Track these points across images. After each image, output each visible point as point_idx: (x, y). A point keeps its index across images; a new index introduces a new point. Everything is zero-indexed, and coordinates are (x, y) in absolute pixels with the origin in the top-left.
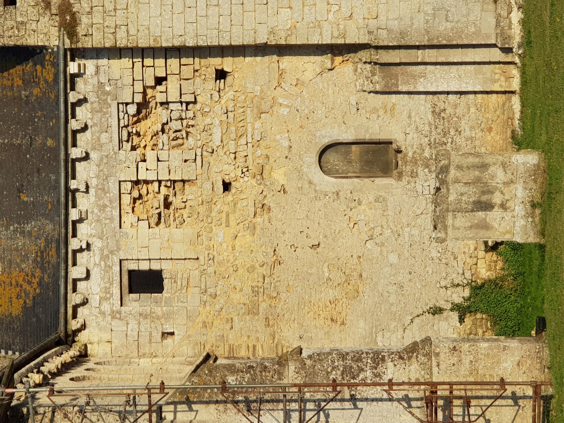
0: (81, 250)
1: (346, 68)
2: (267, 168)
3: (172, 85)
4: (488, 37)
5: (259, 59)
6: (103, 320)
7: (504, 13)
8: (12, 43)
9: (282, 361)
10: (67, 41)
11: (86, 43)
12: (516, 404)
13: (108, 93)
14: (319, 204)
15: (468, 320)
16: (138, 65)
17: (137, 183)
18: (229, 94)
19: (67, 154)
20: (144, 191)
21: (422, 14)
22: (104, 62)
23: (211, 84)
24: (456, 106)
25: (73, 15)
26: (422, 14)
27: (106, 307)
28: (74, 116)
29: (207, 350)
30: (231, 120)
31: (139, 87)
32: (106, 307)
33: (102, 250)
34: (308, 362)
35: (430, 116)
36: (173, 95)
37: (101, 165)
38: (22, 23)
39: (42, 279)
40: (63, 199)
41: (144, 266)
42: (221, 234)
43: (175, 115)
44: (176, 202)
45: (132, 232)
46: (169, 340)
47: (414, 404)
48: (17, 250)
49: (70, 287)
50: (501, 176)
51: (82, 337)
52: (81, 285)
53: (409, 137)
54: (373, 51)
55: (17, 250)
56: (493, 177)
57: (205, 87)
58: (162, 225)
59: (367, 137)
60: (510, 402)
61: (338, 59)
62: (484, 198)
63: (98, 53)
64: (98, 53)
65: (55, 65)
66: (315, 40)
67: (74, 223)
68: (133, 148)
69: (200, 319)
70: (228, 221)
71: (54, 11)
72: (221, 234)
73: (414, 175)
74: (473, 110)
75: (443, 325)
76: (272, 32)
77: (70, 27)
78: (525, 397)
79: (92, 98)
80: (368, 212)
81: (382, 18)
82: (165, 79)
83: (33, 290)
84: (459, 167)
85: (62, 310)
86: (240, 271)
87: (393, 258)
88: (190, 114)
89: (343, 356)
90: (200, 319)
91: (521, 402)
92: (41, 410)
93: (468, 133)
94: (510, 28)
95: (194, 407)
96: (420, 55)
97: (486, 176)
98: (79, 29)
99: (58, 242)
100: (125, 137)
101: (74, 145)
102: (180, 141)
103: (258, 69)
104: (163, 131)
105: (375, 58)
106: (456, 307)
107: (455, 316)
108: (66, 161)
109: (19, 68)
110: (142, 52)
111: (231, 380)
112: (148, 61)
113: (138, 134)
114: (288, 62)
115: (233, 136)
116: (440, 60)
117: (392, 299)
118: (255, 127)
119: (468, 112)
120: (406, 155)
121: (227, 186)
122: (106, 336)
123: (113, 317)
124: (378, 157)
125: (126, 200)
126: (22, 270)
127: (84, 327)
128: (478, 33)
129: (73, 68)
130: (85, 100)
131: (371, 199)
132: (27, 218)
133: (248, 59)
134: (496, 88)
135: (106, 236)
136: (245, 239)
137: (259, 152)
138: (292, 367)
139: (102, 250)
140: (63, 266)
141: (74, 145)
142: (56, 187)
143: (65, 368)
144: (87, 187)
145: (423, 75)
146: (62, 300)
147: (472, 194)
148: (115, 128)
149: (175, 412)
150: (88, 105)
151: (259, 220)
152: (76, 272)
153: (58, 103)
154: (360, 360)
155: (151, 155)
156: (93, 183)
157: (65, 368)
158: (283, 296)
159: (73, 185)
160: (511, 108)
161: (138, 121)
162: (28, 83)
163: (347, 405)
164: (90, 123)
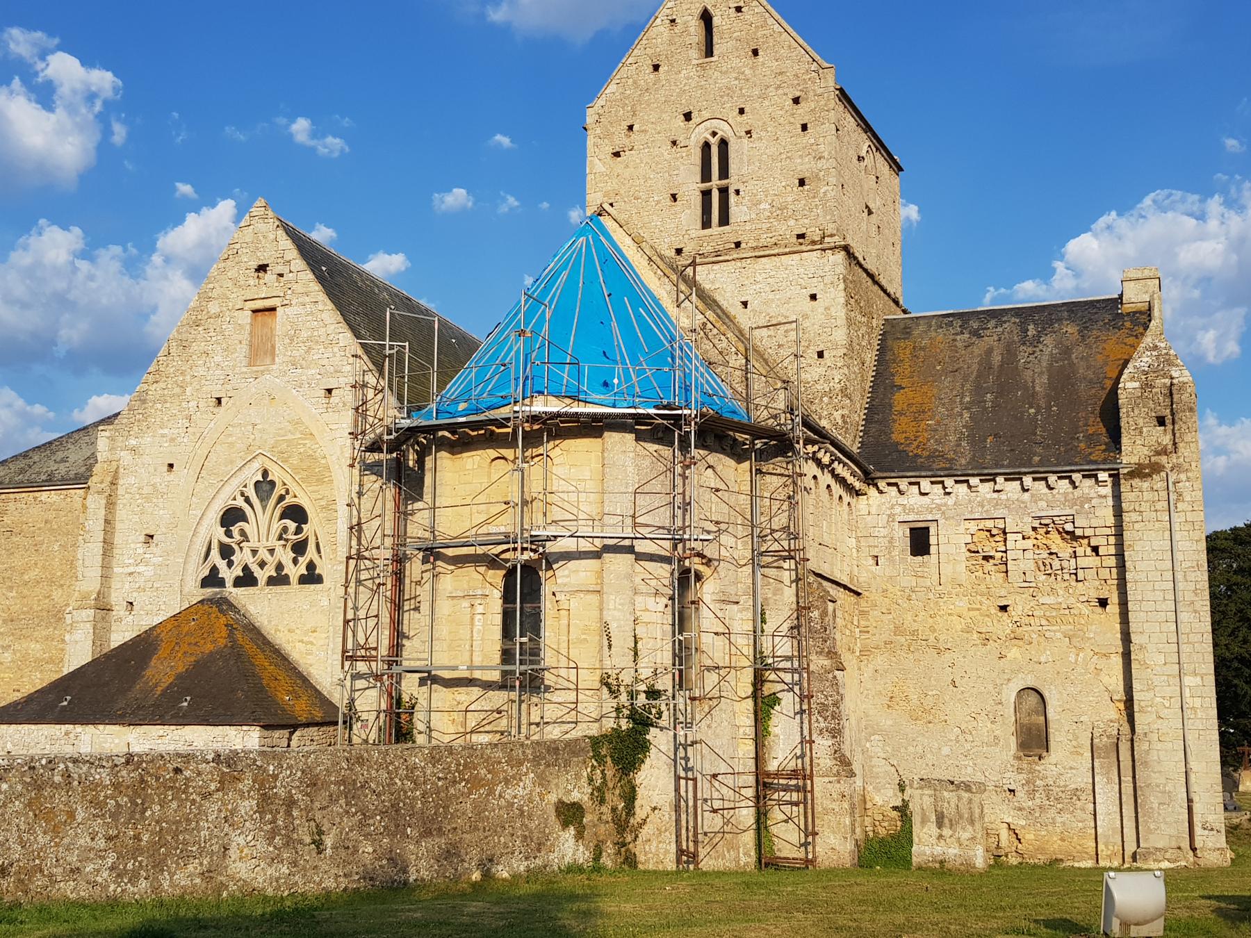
0: (944, 488)
1: (1113, 712)
2: (1021, 643)
3: (1092, 561)
4: (1146, 840)
5: (1119, 636)
6: (889, 507)
7: (1168, 855)
8: (1122, 424)
9: (832, 654)
10: (1126, 471)
11: (1125, 486)
12: (801, 845)
13: (1082, 507)
14: (990, 687)
15: (895, 814)
16: (1108, 531)
17: (1005, 533)
18: (1085, 610)
19: (1025, 474)
20: (997, 538)
21: (1164, 781)
22: (1110, 502)
23: (1094, 595)
24: (1083, 809)
25: (1150, 475)
26: (1164, 781)
27: (898, 510)
28: (1059, 478)
29: (864, 593)
30: (1062, 612)
31: (1088, 532)
32: (898, 510)
33: (946, 505)
34: (830, 676)
35: (1073, 786)
36: (1082, 562)
37: (1019, 502)
38: (1141, 432)
39: (921, 457)
40: (986, 471)
41: (933, 540)
42: (962, 604)
43: (1065, 564)
44: (989, 566)
45: (962, 529)
46: (872, 562)
47: (799, 761)
48: (946, 435)
49: (913, 480)
50: (965, 835)
51: (872, 491)
52: (915, 489)
53: (1053, 768)
54: (1129, 737)
55: (946, 435)
56: (963, 829)
57: (1092, 589)
58: (969, 554)
59: (1051, 730)
60: (803, 840)
61: (1122, 706)
62: (946, 821)
63: (1117, 496)
64: (1117, 496)
65: (1104, 461)
66: (1136, 685)
67: (967, 481)
68: (1034, 529)
69: (890, 587)
70: (973, 609)
71: (1153, 459)
72: (962, 604)
73: (1019, 770)
74: (1080, 825)
75: (890, 793)
76: (1141, 647)
77: (1139, 472)
78: (807, 853)
79: (1077, 493)
80: (985, 730)
81: (1159, 746)
82: (1097, 555)
83: (912, 449)
84: (970, 801)
85: (893, 474)
86: (931, 620)
87: (946, 750)
88: (1066, 577)
89: (836, 704)
90: (890, 587)
91: (803, 849)
92: (790, 466)
93: (1059, 820)
94: (1155, 860)
95: (794, 585)
96: (1127, 779)
97: (964, 823)
98: (1137, 480)
99: (950, 469)
100: (1043, 522)
101: (1034, 479)
102: (1042, 568)
103: (1109, 635)
104: (1051, 554)
105: (1123, 738)
106: (905, 804)
107: (899, 803)
108: (1019, 473)
109: (1104, 430)
110: (1119, 535)
111: (815, 614)
112: (1112, 540)
113: (1048, 532)
114: (1117, 661)
115: (1048, 614)
116: (1124, 797)
117: (911, 749)
118: (1056, 631)
119: (1077, 821)
120: (1037, 764)
121: (1004, 608)
122: (873, 511)
123: (889, 516)
124: (1034, 740)
125: (989, 524)
126: (928, 440)
127: (881, 492)
128: (1149, 831)
129: (1103, 476)
130: (1075, 487)
131: (997, 733)
132: (972, 443)
133: (1118, 626)
134: (1101, 847)
135: (957, 508)
136: (959, 625)
137: (1034, 636)
138: (827, 663)
139: (946, 505)
140: (930, 473)
141: (1034, 479)
142: (997, 466)
143: (842, 481)
144: (999, 491)
145: (1109, 781)
146: (901, 474)
147: (949, 810)
148: (1051, 513)
149: (790, 570)
150: (1071, 490)
151: (975, 636)
152: (925, 484)
153: (1070, 464)
154: (833, 718)
155: (1029, 544)
156: (1003, 496)
157: (842, 481)
158: (911, 656)
159: (1000, 479)
160: (1083, 859)
161: (1060, 533)
162: (1090, 439)
163: (797, 707)
164: (1054, 492)
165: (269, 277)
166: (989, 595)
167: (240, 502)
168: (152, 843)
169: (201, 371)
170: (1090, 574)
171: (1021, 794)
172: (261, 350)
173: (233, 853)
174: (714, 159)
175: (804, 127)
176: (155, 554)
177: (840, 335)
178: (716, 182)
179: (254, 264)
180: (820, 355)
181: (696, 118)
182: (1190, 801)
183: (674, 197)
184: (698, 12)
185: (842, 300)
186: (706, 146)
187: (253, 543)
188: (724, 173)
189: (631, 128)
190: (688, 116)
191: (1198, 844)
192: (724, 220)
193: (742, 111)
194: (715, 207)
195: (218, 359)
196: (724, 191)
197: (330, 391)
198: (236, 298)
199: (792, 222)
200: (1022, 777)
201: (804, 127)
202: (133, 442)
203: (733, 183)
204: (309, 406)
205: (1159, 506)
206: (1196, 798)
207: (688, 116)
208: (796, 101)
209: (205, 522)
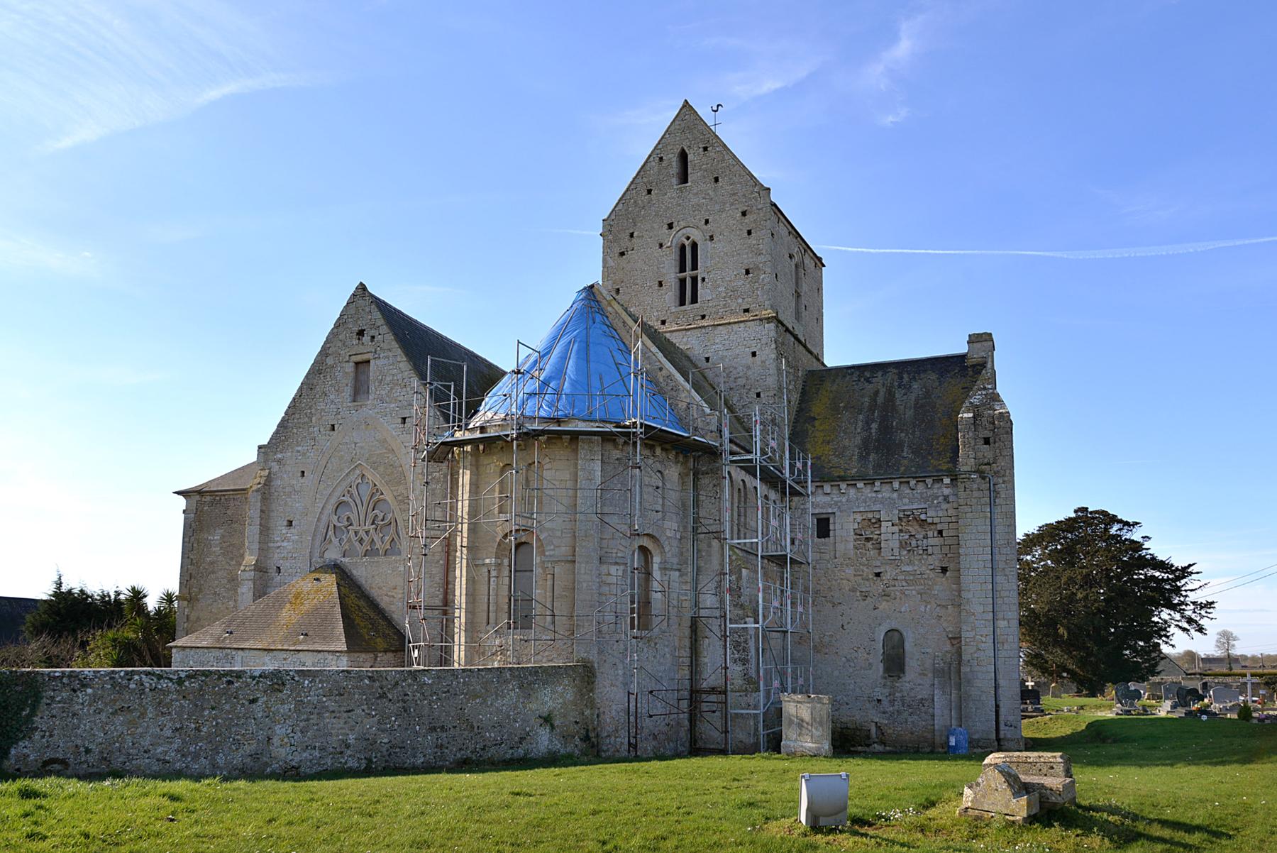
18: (932, 575)
31: (936, 520)
37: (887, 500)
44: (869, 545)
72: (850, 571)
121: (878, 575)
125: (870, 516)
136: (847, 586)
155: (896, 529)
159: (877, 483)
165: (366, 339)
166: (868, 566)
167: (347, 498)
168: (209, 734)
169: (322, 406)
170: (937, 550)
171: (885, 702)
172: (359, 390)
173: (276, 740)
174: (688, 256)
175: (749, 232)
176: (293, 534)
177: (771, 381)
178: (689, 273)
179: (356, 329)
180: (758, 395)
181: (676, 228)
182: (997, 706)
183: (660, 284)
184: (677, 151)
185: (774, 356)
186: (683, 247)
187: (355, 527)
188: (695, 267)
189: (632, 235)
190: (670, 226)
191: (1002, 736)
192: (694, 300)
193: (707, 222)
194: (688, 292)
195: (332, 397)
196: (694, 280)
197: (404, 419)
198: (344, 353)
199: (740, 301)
200: (886, 691)
201: (749, 232)
202: (279, 456)
203: (700, 273)
204: (390, 428)
205: (983, 501)
206: (1001, 705)
207: (670, 226)
208: (744, 214)
209: (326, 512)
